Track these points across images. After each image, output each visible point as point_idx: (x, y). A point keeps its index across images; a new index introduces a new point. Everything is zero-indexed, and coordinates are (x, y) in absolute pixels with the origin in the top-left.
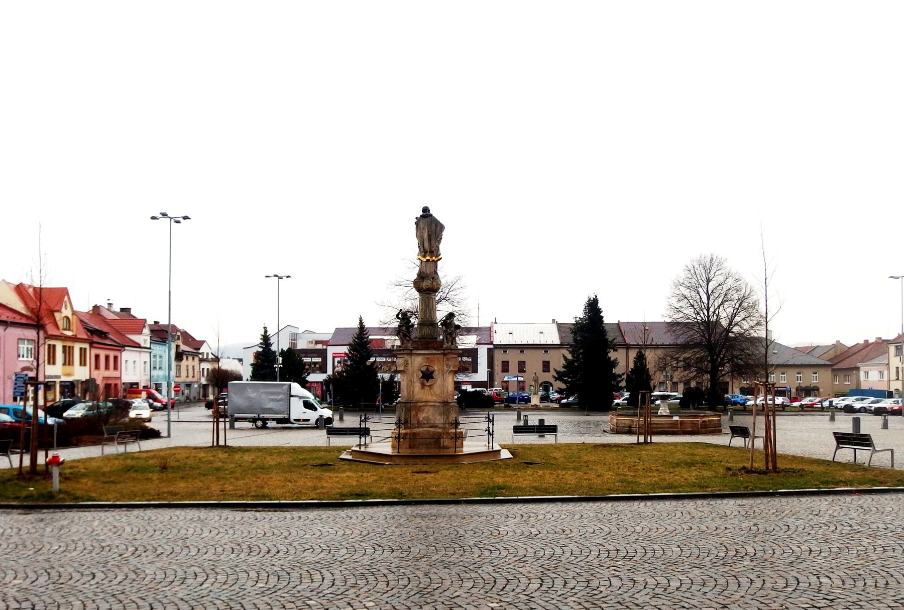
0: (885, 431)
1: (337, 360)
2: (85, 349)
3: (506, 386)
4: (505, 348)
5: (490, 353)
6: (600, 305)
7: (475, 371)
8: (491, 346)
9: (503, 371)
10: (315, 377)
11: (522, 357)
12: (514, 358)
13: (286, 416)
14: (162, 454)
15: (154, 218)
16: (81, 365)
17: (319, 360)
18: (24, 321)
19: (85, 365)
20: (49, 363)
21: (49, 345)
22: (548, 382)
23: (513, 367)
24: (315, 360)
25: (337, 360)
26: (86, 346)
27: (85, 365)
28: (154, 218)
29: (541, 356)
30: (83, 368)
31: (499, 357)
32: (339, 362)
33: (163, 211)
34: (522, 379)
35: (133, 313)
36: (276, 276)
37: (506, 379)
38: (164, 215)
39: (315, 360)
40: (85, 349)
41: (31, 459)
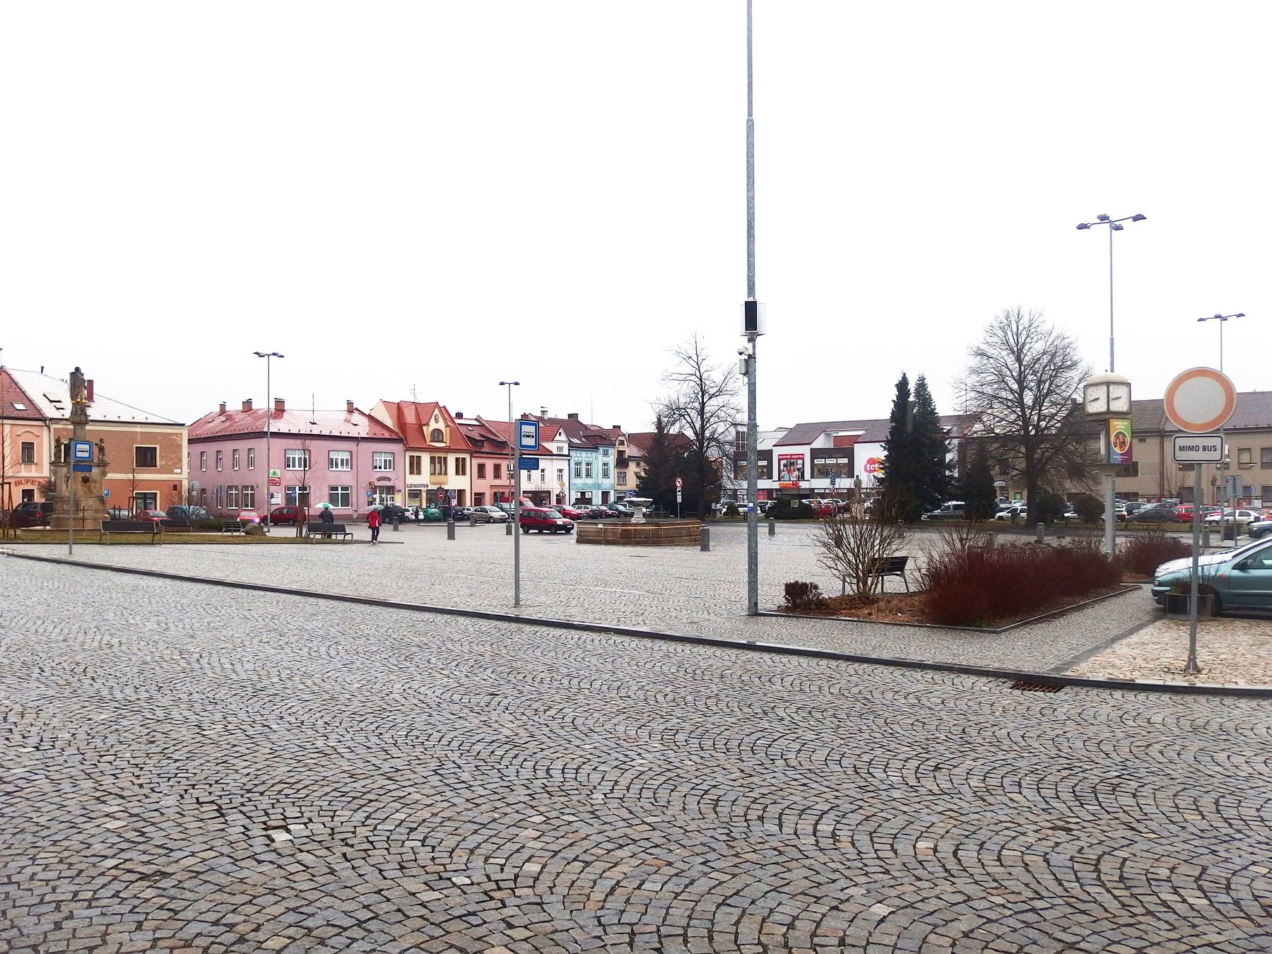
0: (451, 542)
1: (783, 462)
2: (464, 459)
10: (1015, 473)
14: (148, 537)
15: (1082, 227)
16: (457, 473)
17: (845, 461)
18: (387, 435)
19: (464, 474)
20: (412, 473)
21: (411, 457)
24: (841, 461)
25: (783, 462)
26: (467, 456)
27: (464, 474)
28: (1082, 227)
30: (461, 477)
33: (1101, 213)
35: (580, 419)
36: (1217, 317)
38: (1104, 218)
39: (841, 461)
40: (464, 459)
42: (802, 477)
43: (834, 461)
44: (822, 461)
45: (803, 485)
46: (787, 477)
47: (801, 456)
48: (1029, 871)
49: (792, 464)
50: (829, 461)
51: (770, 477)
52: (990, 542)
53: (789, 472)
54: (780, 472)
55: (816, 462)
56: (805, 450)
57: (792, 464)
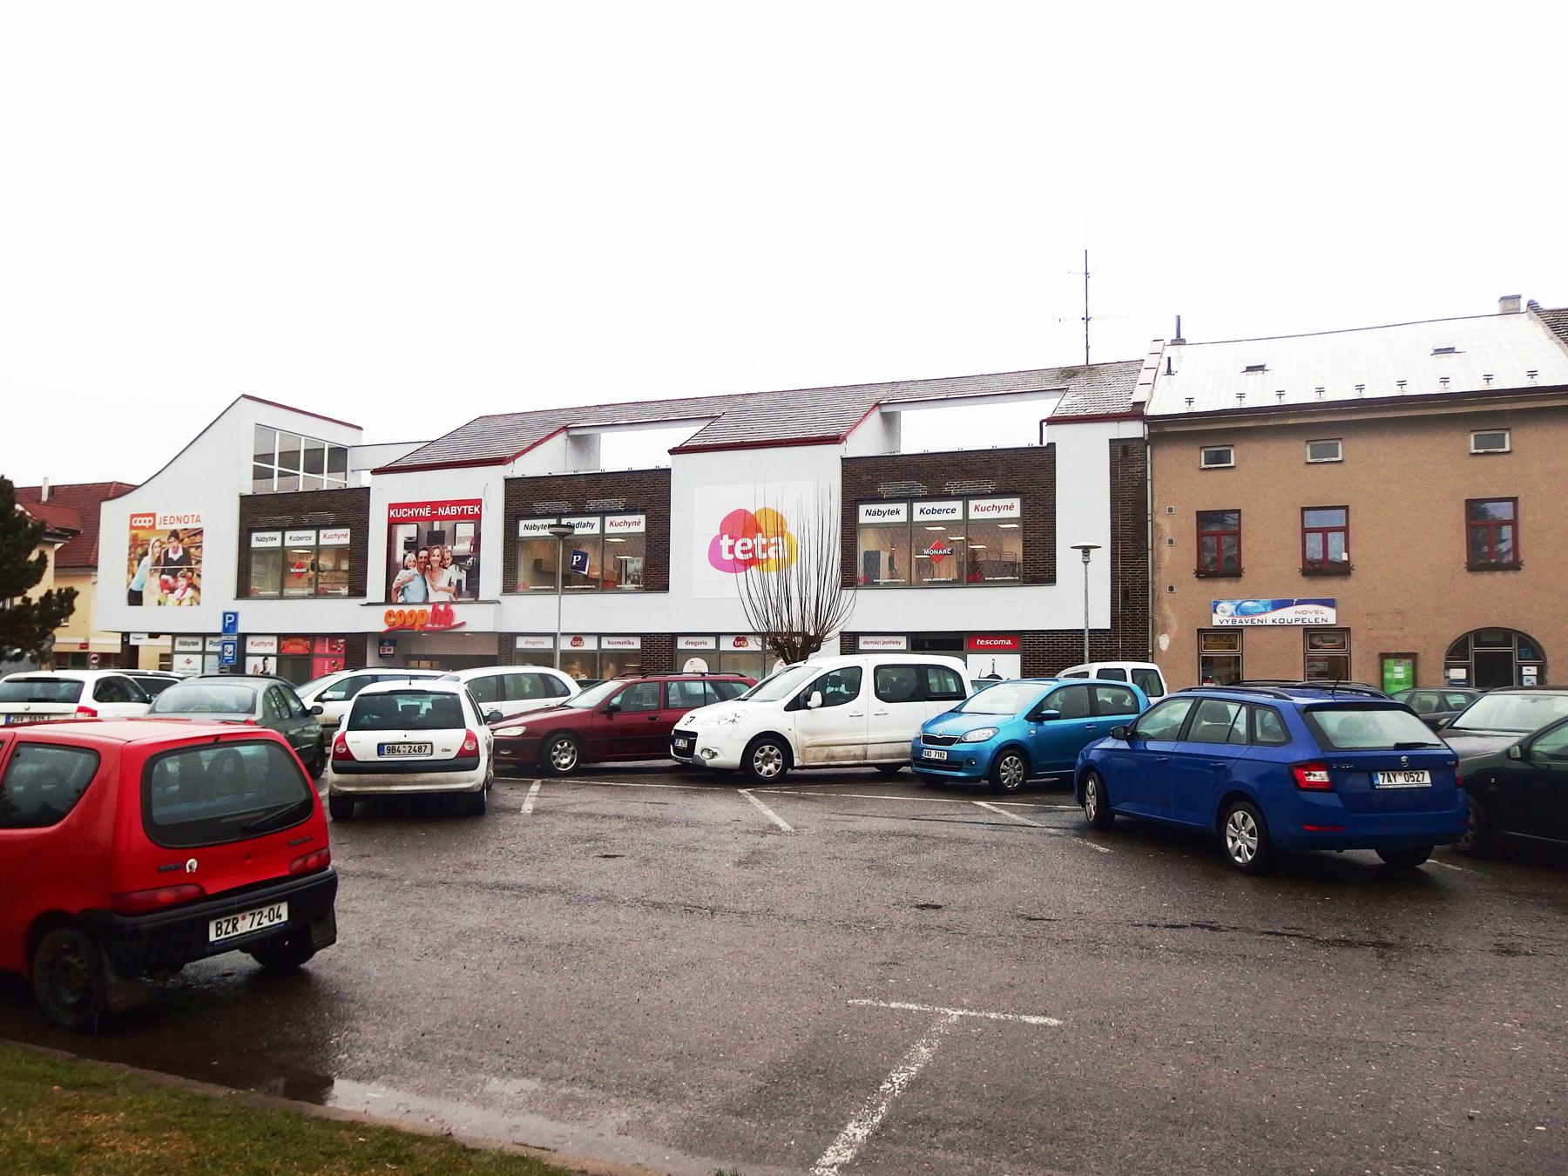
1: (405, 532)
3: (1221, 657)
4: (1215, 433)
5: (1123, 456)
6: (77, 602)
7: (1038, 568)
8: (1135, 430)
9: (1203, 573)
11: (1324, 484)
12: (1265, 487)
13: (884, 578)
17: (637, 524)
22: (1506, 635)
23: (1269, 545)
29: (1452, 469)
31: (1181, 488)
32: (410, 545)
34: (1328, 616)
37: (1223, 616)
40: (1038, 568)
41: (856, 514)
42: (470, 588)
43: (951, 510)
44: (898, 513)
45: (471, 618)
46: (415, 590)
47: (470, 511)
48: (585, 901)
49: (437, 539)
50: (924, 512)
51: (358, 590)
52: (27, 601)
53: (425, 569)
54: (391, 569)
55: (865, 514)
56: (487, 487)
57: (437, 539)
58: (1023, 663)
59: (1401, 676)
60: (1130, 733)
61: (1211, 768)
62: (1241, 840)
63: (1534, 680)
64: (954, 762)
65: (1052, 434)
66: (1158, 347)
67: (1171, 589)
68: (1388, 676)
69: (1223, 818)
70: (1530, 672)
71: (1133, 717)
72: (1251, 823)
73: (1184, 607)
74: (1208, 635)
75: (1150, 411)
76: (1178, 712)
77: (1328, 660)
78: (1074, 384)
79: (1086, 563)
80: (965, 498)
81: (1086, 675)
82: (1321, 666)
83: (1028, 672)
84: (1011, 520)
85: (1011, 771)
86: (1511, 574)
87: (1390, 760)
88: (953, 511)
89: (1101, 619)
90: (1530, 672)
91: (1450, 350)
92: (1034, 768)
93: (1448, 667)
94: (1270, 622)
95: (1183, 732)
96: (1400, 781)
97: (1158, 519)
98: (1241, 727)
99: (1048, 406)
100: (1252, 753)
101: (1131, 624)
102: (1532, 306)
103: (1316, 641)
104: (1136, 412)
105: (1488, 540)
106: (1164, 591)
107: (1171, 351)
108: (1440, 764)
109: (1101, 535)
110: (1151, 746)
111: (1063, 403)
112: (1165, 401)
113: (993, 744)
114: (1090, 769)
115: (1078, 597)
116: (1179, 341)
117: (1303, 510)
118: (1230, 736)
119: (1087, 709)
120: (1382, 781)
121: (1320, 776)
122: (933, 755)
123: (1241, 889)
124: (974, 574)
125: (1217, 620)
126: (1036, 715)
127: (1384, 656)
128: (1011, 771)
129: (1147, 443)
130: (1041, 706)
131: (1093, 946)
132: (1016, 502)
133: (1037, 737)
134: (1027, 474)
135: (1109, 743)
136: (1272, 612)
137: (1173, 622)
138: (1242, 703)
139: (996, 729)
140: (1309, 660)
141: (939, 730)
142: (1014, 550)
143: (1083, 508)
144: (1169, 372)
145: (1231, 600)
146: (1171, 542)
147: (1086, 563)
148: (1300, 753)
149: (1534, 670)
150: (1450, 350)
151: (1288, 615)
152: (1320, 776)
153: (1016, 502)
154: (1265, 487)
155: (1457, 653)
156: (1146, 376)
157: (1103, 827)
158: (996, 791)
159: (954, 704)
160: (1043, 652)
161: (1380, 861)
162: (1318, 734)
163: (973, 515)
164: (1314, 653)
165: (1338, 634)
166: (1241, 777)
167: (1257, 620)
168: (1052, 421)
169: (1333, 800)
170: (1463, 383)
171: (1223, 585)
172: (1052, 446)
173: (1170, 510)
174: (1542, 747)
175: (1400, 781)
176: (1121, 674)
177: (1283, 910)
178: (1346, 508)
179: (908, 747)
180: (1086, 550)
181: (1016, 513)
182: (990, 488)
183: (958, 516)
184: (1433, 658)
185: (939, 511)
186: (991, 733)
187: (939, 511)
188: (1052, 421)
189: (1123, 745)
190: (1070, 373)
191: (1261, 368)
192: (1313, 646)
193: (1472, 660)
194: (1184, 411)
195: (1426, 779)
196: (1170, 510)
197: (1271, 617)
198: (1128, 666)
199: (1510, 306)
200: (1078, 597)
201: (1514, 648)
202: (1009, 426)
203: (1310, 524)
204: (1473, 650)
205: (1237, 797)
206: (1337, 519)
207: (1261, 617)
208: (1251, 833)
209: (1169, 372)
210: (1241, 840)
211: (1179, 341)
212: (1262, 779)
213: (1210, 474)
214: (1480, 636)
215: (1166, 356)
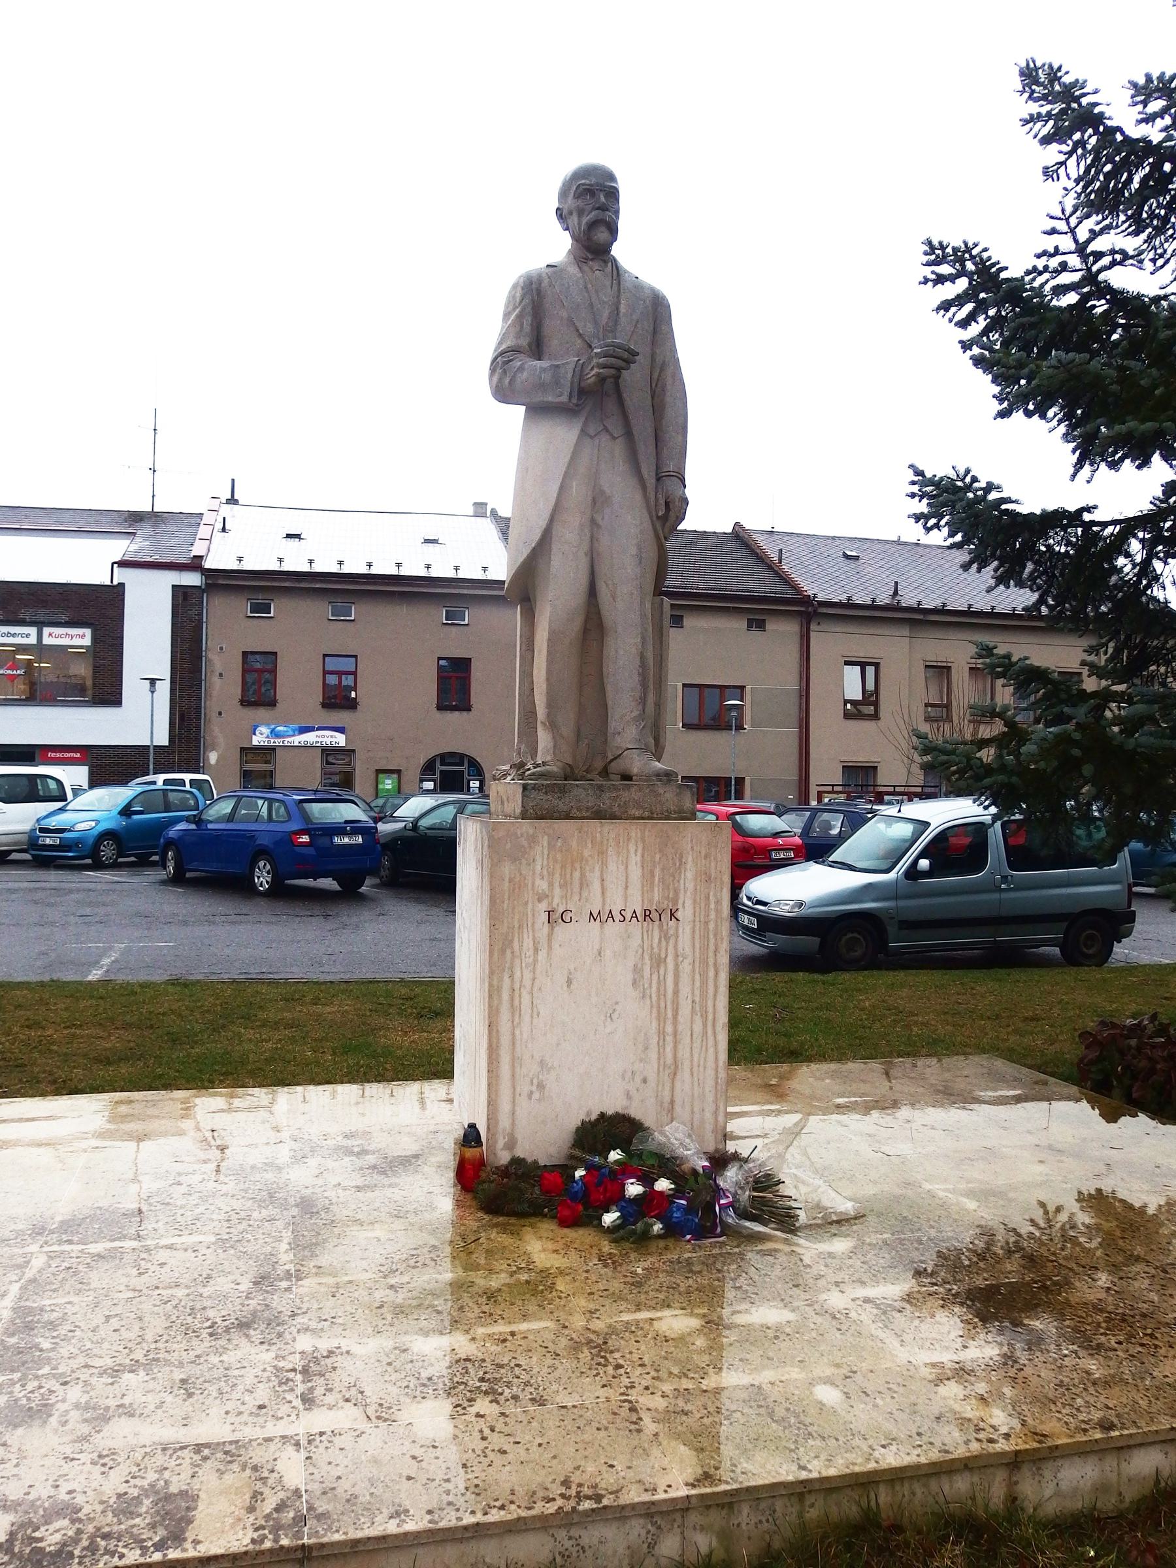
3: (257, 768)
7: (105, 689)
8: (193, 579)
9: (245, 702)
22: (459, 758)
23: (299, 681)
31: (230, 633)
34: (340, 740)
40: (105, 689)
43: (26, 635)
58: (91, 774)
59: (390, 787)
60: (198, 821)
61: (247, 837)
62: (263, 879)
63: (477, 791)
64: (64, 846)
65: (120, 576)
66: (215, 504)
67: (220, 713)
68: (380, 786)
69: (253, 865)
70: (475, 784)
71: (195, 813)
72: (268, 867)
73: (230, 729)
74: (249, 752)
75: (208, 564)
76: (226, 807)
77: (338, 772)
78: (145, 529)
79: (153, 692)
80: (40, 625)
81: (154, 783)
82: (336, 779)
83: (95, 782)
84: (81, 647)
85: (107, 851)
86: (465, 713)
87: (340, 830)
88: (28, 635)
89: (162, 739)
90: (475, 784)
91: (435, 541)
92: (127, 847)
93: (422, 781)
94: (296, 744)
95: (231, 818)
96: (346, 840)
97: (210, 655)
98: (264, 812)
99: (119, 548)
100: (271, 827)
101: (186, 744)
102: (493, 511)
103: (331, 759)
104: (195, 564)
105: (454, 684)
106: (215, 715)
107: (226, 510)
108: (368, 832)
109: (162, 668)
110: (210, 826)
111: (133, 547)
112: (220, 559)
113: (95, 832)
114: (170, 843)
115: (140, 717)
116: (232, 501)
117: (325, 656)
118: (258, 818)
119: (162, 808)
120: (337, 840)
121: (305, 839)
122: (48, 841)
123: (263, 902)
124: (37, 694)
125: (257, 740)
126: (126, 811)
127: (379, 772)
128: (107, 851)
129: (204, 591)
130: (129, 805)
131: (185, 923)
132: (88, 632)
133: (126, 828)
134: (99, 607)
135: (182, 826)
136: (301, 736)
137: (221, 740)
138: (265, 799)
139: (98, 822)
140: (325, 774)
141: (53, 822)
142: (82, 670)
143: (147, 644)
144: (224, 530)
145: (267, 724)
146: (221, 675)
147: (153, 692)
148: (294, 826)
149: (477, 784)
150: (435, 541)
151: (311, 738)
152: (305, 839)
153: (88, 632)
154: (299, 640)
155: (428, 769)
156: (204, 531)
157: (178, 880)
158: (98, 865)
159: (60, 805)
160: (110, 766)
161: (339, 888)
162: (306, 817)
163: (47, 640)
164: (330, 768)
165: (347, 753)
166: (264, 841)
167: (287, 741)
168: (123, 564)
169: (311, 851)
170: (441, 570)
171: (262, 712)
172: (122, 585)
173: (221, 648)
174: (424, 823)
175: (346, 840)
176: (182, 782)
177: (280, 907)
178: (356, 657)
179: (25, 838)
180: (153, 682)
181: (87, 641)
182: (64, 618)
183: (33, 640)
184: (412, 772)
185: (13, 635)
186: (93, 824)
187: (13, 635)
188: (123, 564)
189: (193, 827)
190: (136, 518)
191: (298, 536)
192: (328, 763)
193: (438, 775)
194: (235, 568)
195: (360, 839)
196: (221, 648)
197: (298, 740)
198: (187, 777)
199: (480, 510)
200: (140, 717)
201: (465, 768)
202: (84, 563)
203: (329, 668)
204: (439, 767)
205: (262, 852)
206: (348, 665)
207: (290, 739)
208: (268, 873)
209: (224, 530)
210: (263, 879)
211: (232, 501)
212: (277, 843)
213: (256, 621)
214: (444, 758)
215: (222, 514)
